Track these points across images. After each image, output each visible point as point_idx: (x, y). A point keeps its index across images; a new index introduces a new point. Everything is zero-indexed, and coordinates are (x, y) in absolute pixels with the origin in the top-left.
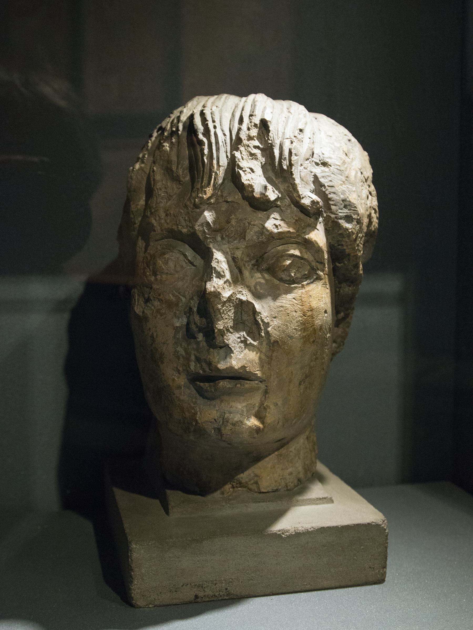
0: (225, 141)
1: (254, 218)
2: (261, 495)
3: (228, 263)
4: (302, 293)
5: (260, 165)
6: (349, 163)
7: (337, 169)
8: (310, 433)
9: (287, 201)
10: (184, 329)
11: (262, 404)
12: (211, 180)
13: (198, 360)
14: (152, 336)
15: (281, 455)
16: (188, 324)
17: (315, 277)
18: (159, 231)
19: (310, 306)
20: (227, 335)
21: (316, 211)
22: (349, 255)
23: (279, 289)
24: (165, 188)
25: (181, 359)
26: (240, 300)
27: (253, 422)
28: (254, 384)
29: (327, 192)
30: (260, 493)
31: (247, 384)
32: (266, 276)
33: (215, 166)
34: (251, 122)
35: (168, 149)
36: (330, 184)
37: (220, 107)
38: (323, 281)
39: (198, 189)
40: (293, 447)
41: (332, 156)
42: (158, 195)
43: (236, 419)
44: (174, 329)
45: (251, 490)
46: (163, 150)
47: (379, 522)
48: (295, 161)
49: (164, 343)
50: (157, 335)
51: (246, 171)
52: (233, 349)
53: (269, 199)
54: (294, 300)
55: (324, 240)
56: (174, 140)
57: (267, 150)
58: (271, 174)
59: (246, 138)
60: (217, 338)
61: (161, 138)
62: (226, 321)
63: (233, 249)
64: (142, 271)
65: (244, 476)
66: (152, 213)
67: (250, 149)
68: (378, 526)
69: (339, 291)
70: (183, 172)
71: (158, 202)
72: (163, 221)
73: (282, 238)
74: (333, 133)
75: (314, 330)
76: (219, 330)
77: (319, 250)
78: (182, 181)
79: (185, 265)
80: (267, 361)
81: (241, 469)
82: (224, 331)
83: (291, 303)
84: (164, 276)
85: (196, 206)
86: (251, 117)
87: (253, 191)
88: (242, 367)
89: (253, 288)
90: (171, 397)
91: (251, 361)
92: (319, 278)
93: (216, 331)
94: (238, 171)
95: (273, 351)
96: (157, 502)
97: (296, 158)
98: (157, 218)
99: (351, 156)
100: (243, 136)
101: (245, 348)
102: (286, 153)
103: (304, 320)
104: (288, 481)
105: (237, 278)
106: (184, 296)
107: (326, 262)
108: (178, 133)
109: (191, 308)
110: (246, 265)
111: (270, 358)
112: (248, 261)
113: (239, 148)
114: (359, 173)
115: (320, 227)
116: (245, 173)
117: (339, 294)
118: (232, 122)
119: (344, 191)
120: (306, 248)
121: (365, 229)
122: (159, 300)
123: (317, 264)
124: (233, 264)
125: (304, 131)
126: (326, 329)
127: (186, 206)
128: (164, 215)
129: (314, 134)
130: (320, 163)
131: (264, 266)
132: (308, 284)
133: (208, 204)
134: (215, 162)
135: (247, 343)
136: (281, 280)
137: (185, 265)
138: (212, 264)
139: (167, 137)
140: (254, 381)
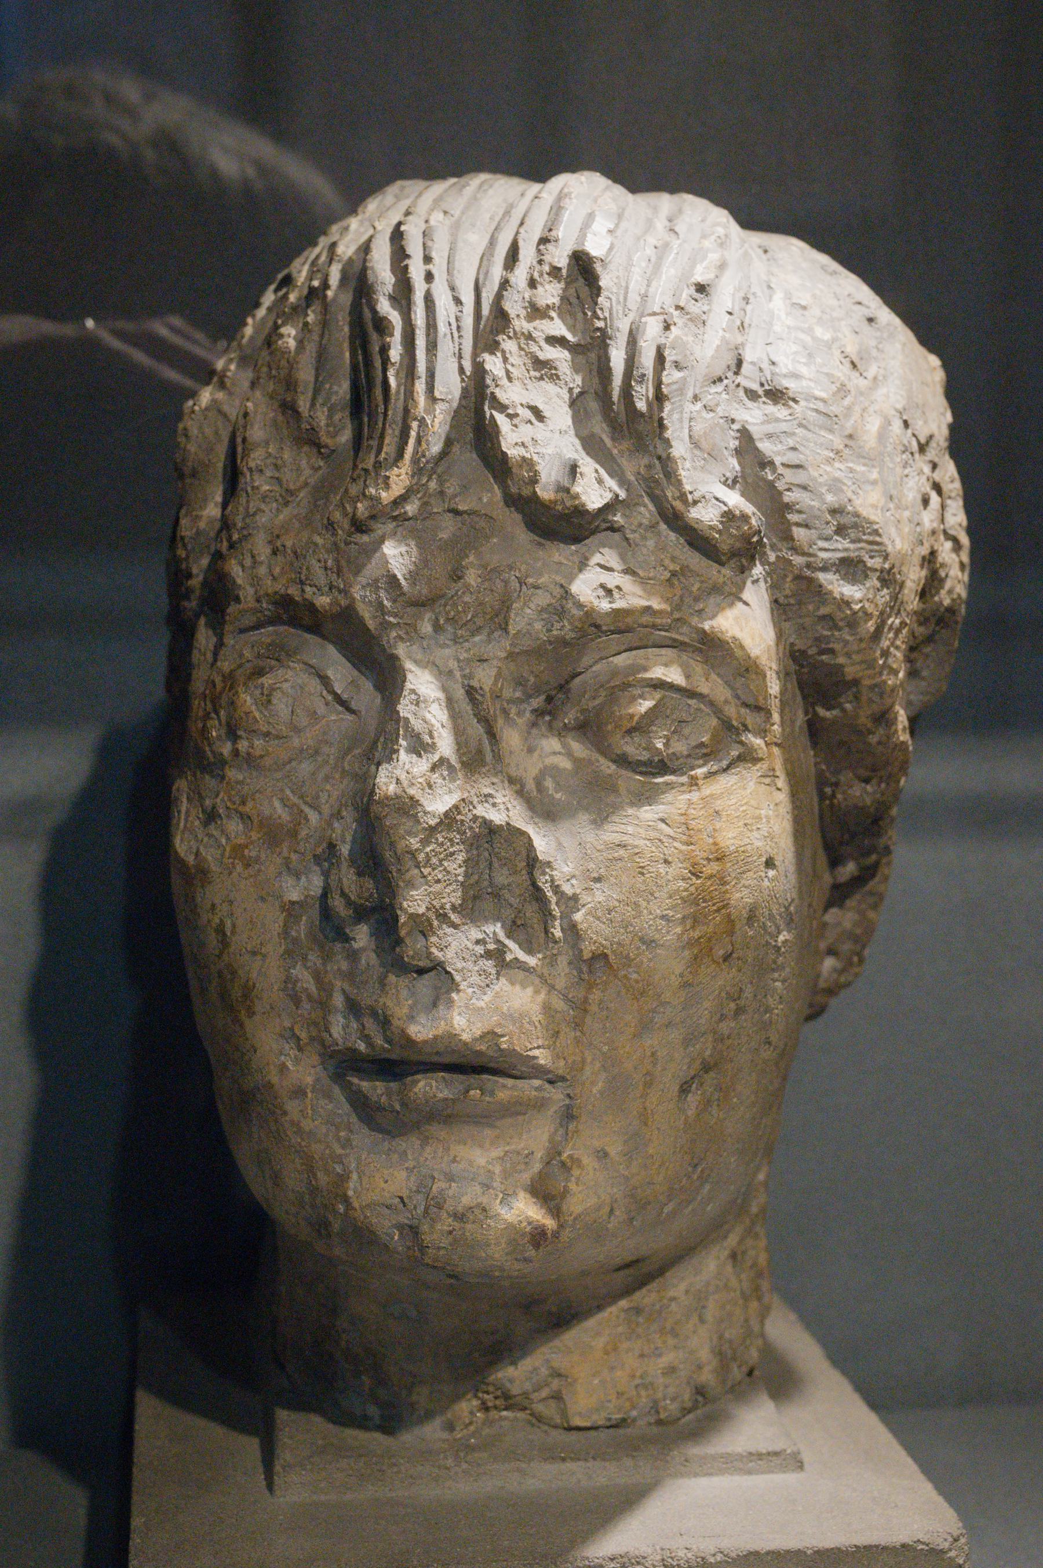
0: (457, 319)
1: (539, 564)
2: (574, 1436)
3: (450, 702)
4: (690, 803)
5: (567, 397)
6: (862, 394)
7: (817, 411)
8: (742, 1240)
9: (647, 511)
10: (315, 913)
11: (554, 1152)
12: (406, 443)
13: (353, 1008)
14: (220, 930)
15: (638, 1311)
16: (325, 895)
17: (735, 753)
18: (252, 604)
19: (715, 844)
20: (440, 933)
21: (738, 545)
22: (856, 682)
23: (614, 789)
24: (276, 467)
25: (306, 1005)
26: (486, 823)
27: (524, 1210)
28: (530, 1088)
29: (780, 485)
30: (570, 1429)
31: (505, 1090)
32: (578, 748)
33: (421, 399)
34: (540, 262)
35: (292, 344)
36: (793, 458)
37: (457, 213)
38: (764, 766)
39: (366, 471)
40: (679, 1286)
41: (804, 370)
42: (253, 488)
43: (466, 1201)
44: (283, 909)
45: (539, 1418)
46: (279, 349)
47: (940, 1540)
48: (674, 387)
49: (254, 953)
50: (234, 926)
51: (517, 415)
52: (458, 978)
53: (583, 505)
54: (663, 826)
55: (769, 635)
56: (311, 318)
57: (591, 350)
58: (599, 428)
59: (523, 313)
60: (407, 941)
61: (282, 313)
62: (438, 887)
63: (468, 661)
64: (200, 725)
65: (515, 1375)
66: (232, 546)
67: (534, 348)
68: (935, 1553)
69: (834, 796)
70: (330, 417)
71: (252, 511)
72: (262, 570)
73: (624, 628)
74: (814, 296)
75: (730, 921)
76: (414, 917)
77: (747, 669)
78: (326, 446)
79: (321, 709)
80: (574, 1016)
81: (502, 1349)
82: (428, 920)
83: (653, 834)
84: (258, 743)
85: (359, 527)
86: (542, 247)
87: (534, 480)
88: (482, 1037)
89: (530, 785)
90: (276, 1121)
91: (518, 1018)
92: (748, 757)
93: (402, 919)
94: (492, 416)
95: (590, 987)
96: (251, 1446)
97: (677, 375)
98: (248, 562)
99: (872, 371)
100: (513, 307)
101: (498, 974)
102: (647, 361)
103: (692, 889)
104: (660, 1395)
105: (480, 752)
106: (316, 808)
107: (774, 706)
108: (325, 296)
109: (332, 846)
110: (513, 710)
111: (582, 1007)
112: (520, 701)
113: (497, 343)
114: (897, 425)
115: (756, 595)
116: (516, 421)
117: (832, 806)
118: (485, 262)
119: (837, 480)
120: (706, 662)
121: (913, 603)
122: (242, 818)
123: (743, 710)
124: (469, 708)
125: (711, 290)
126: (771, 917)
127: (330, 526)
128: (268, 551)
129: (746, 300)
130: (760, 392)
131: (570, 716)
132: (711, 775)
133: (395, 518)
134: (420, 386)
135: (504, 960)
136: (623, 761)
137: (321, 709)
138: (400, 708)
139: (295, 309)
140: (530, 1078)
